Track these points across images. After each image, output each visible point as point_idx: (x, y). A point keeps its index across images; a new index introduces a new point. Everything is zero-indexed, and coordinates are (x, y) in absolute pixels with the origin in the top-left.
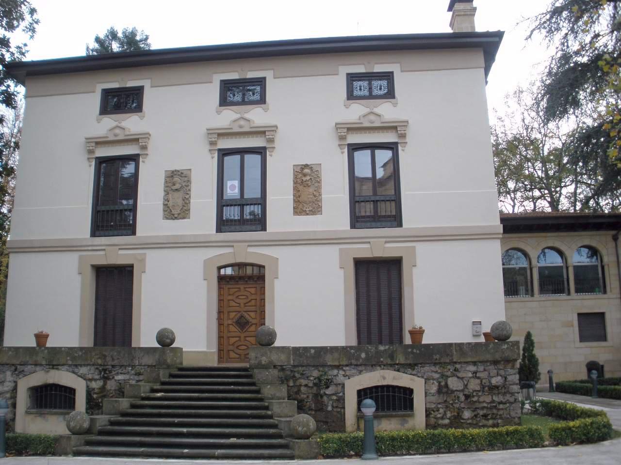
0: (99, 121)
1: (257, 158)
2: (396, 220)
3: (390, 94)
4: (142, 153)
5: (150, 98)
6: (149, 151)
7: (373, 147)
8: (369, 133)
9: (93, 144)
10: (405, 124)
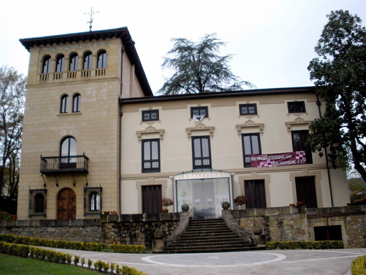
0: (288, 116)
1: (206, 140)
3: (256, 113)
4: (161, 138)
5: (260, 108)
8: (156, 134)
9: (290, 125)
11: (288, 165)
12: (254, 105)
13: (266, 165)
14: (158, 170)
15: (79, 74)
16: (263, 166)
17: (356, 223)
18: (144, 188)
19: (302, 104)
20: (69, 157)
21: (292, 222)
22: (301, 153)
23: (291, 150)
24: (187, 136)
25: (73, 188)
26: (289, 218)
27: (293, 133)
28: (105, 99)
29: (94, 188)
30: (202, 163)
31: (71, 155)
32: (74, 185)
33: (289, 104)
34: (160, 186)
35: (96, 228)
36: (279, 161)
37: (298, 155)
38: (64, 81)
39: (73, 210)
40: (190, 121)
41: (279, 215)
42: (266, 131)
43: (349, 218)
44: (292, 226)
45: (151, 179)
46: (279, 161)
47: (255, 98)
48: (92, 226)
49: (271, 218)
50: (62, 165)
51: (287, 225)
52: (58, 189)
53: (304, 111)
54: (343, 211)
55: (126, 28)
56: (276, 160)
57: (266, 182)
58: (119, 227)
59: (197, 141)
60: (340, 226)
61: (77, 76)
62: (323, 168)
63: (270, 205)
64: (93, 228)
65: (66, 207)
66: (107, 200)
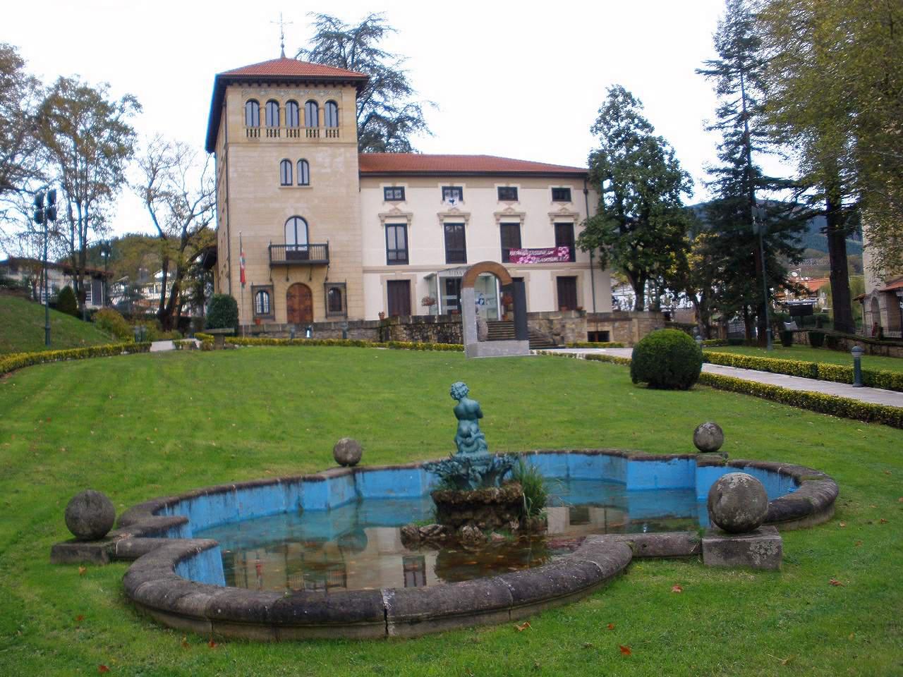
0: (552, 204)
2: (406, 261)
3: (403, 199)
5: (521, 193)
6: (470, 222)
7: (396, 226)
10: (469, 214)
11: (549, 262)
12: (402, 189)
13: (526, 261)
15: (303, 132)
16: (523, 262)
17: (624, 328)
18: (391, 284)
19: (568, 191)
20: (297, 246)
21: (573, 326)
22: (564, 250)
23: (553, 245)
24: (379, 223)
25: (309, 284)
26: (571, 322)
27: (446, 225)
28: (342, 170)
29: (336, 284)
31: (306, 243)
32: (310, 279)
33: (500, 189)
34: (407, 283)
35: (364, 331)
36: (541, 257)
37: (560, 252)
38: (283, 141)
39: (309, 310)
40: (442, 203)
41: (562, 319)
43: (617, 324)
44: (573, 330)
45: (399, 273)
46: (541, 257)
47: (515, 180)
48: (359, 328)
49: (555, 322)
51: (569, 329)
53: (569, 199)
56: (537, 256)
57: (525, 280)
58: (410, 329)
59: (391, 230)
60: (608, 332)
61: (261, 135)
64: (359, 331)
65: (296, 307)
66: (352, 298)
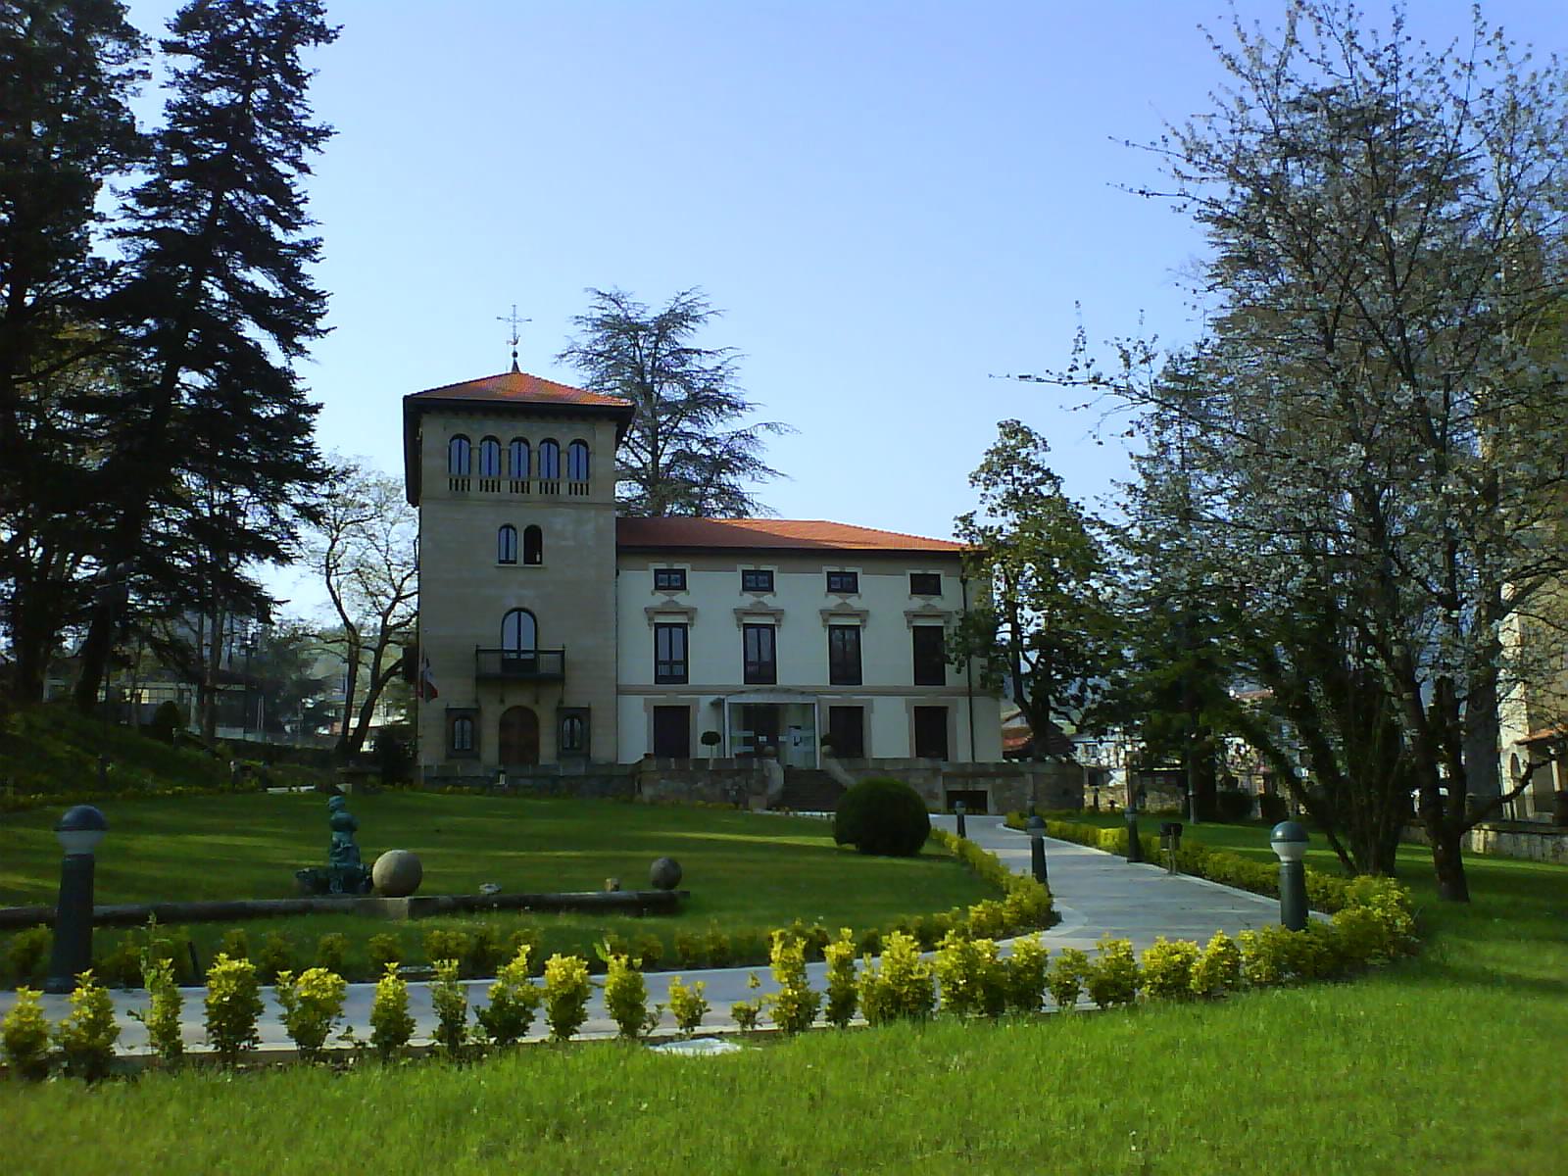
5: (779, 580)
14: (684, 679)
20: (519, 651)
30: (671, 671)
32: (537, 702)
34: (687, 708)
39: (534, 746)
42: (870, 623)
43: (999, 781)
45: (671, 696)
50: (506, 664)
52: (503, 708)
53: (938, 592)
54: (992, 770)
55: (406, 398)
60: (986, 792)
62: (962, 694)
63: (956, 757)
